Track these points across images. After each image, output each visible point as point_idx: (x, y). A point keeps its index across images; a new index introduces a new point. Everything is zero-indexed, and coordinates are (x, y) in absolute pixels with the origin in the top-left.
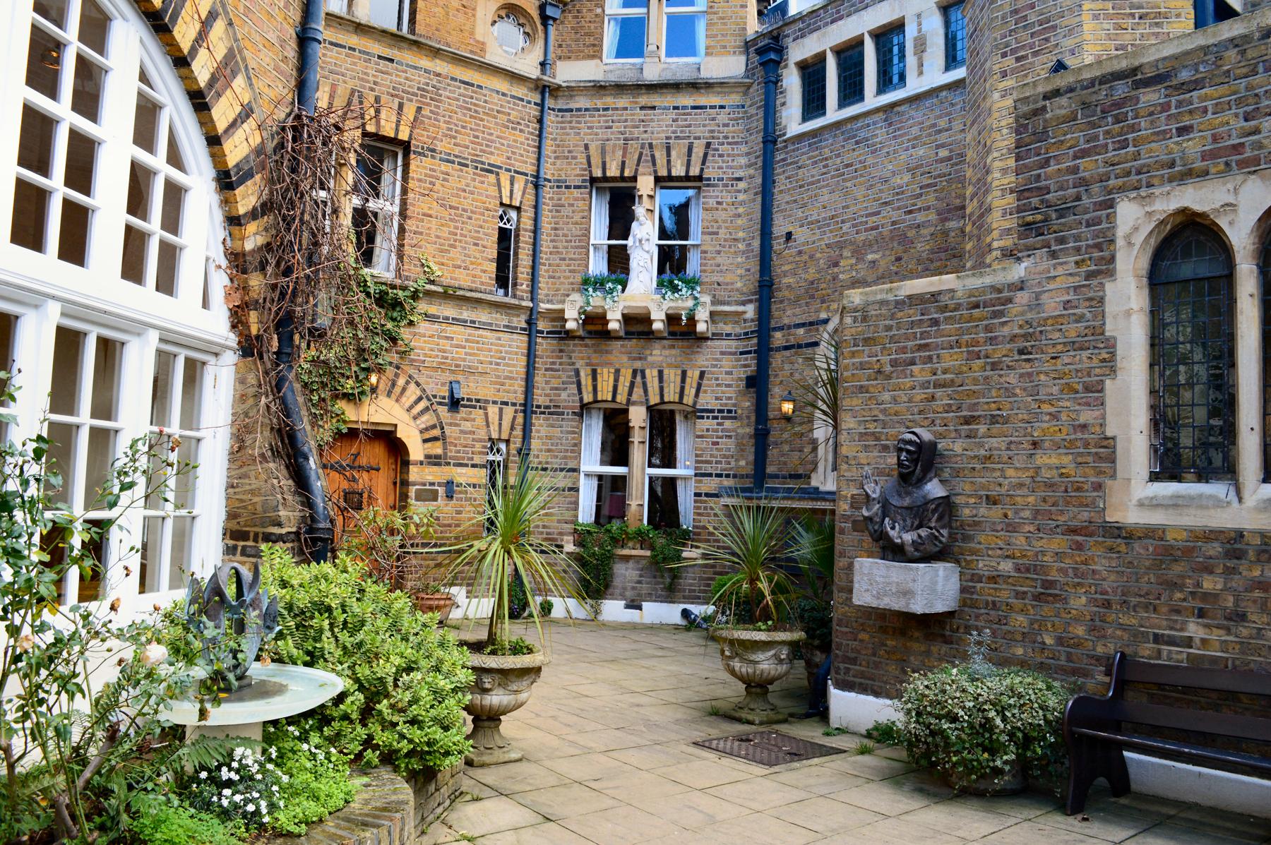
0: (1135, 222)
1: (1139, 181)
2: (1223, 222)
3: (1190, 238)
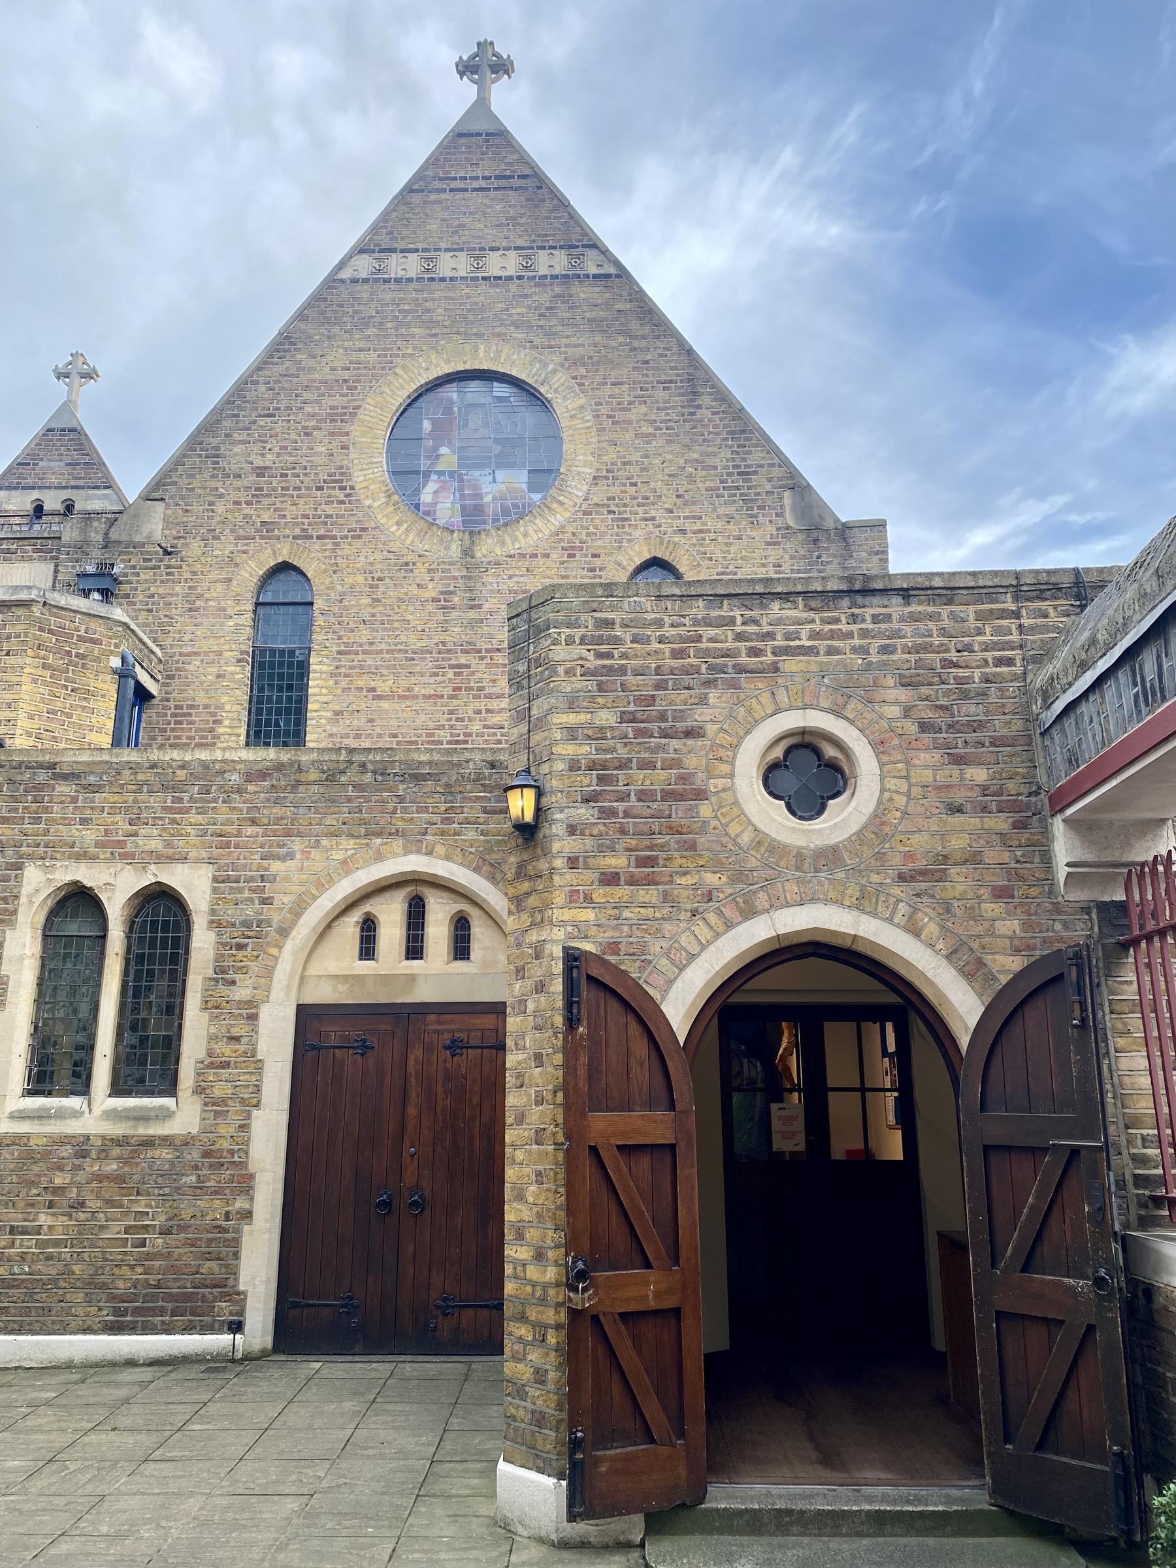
0: (38, 885)
1: (48, 852)
2: (103, 897)
3: (79, 901)
